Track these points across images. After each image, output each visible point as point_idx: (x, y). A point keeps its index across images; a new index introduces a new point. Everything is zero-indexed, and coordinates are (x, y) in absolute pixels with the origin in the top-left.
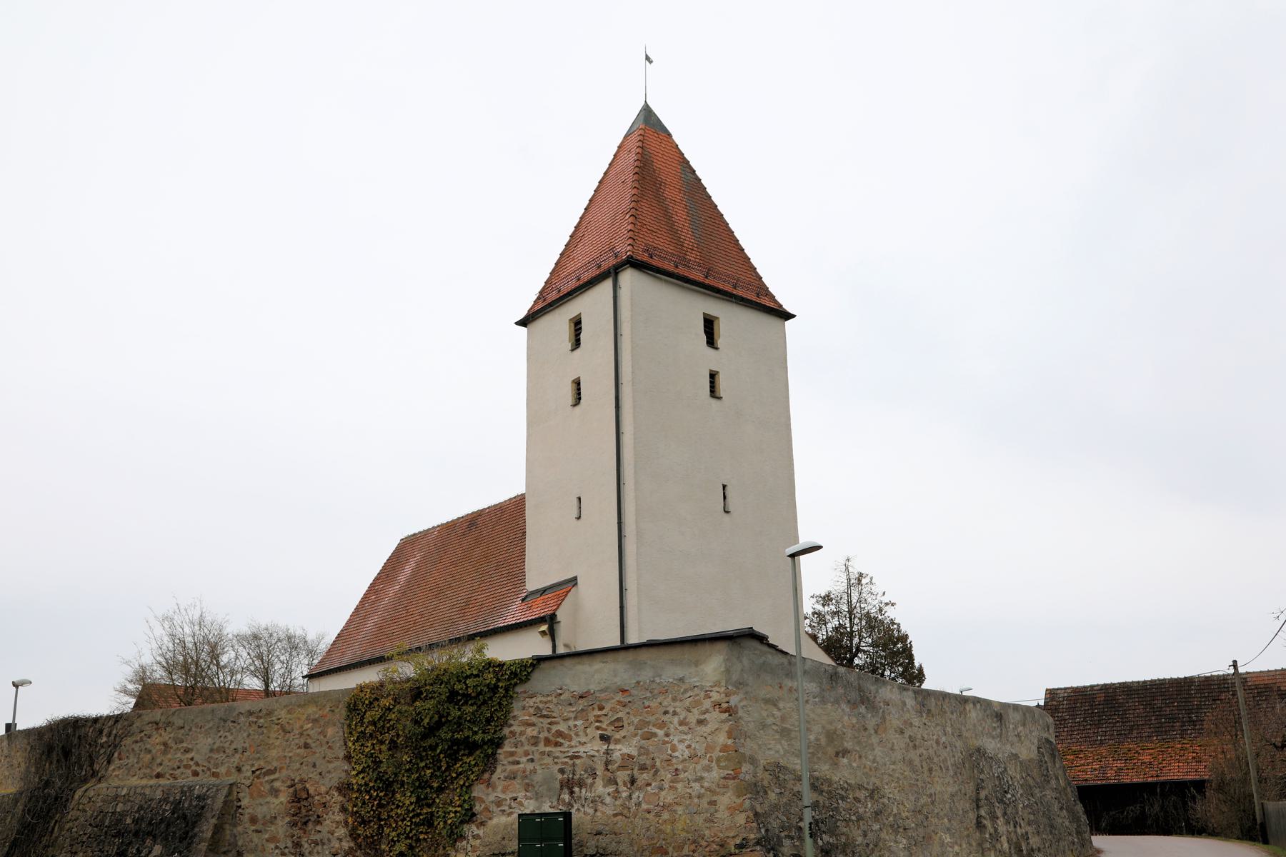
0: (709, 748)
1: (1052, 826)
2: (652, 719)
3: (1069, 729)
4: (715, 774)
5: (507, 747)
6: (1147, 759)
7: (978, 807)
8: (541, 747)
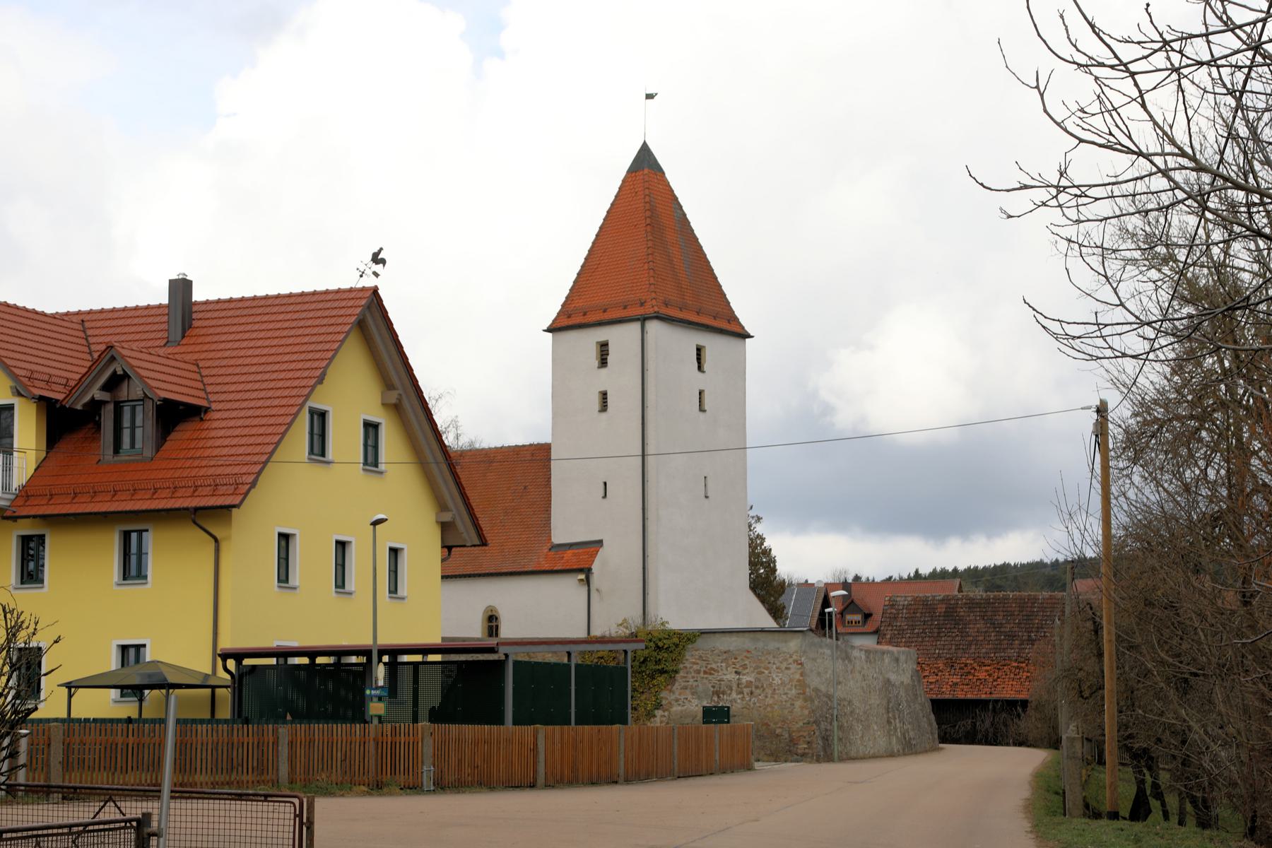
0: (791, 680)
1: (919, 726)
2: (763, 665)
3: (907, 639)
4: (794, 692)
5: (682, 674)
6: (982, 675)
7: (888, 712)
8: (702, 675)
